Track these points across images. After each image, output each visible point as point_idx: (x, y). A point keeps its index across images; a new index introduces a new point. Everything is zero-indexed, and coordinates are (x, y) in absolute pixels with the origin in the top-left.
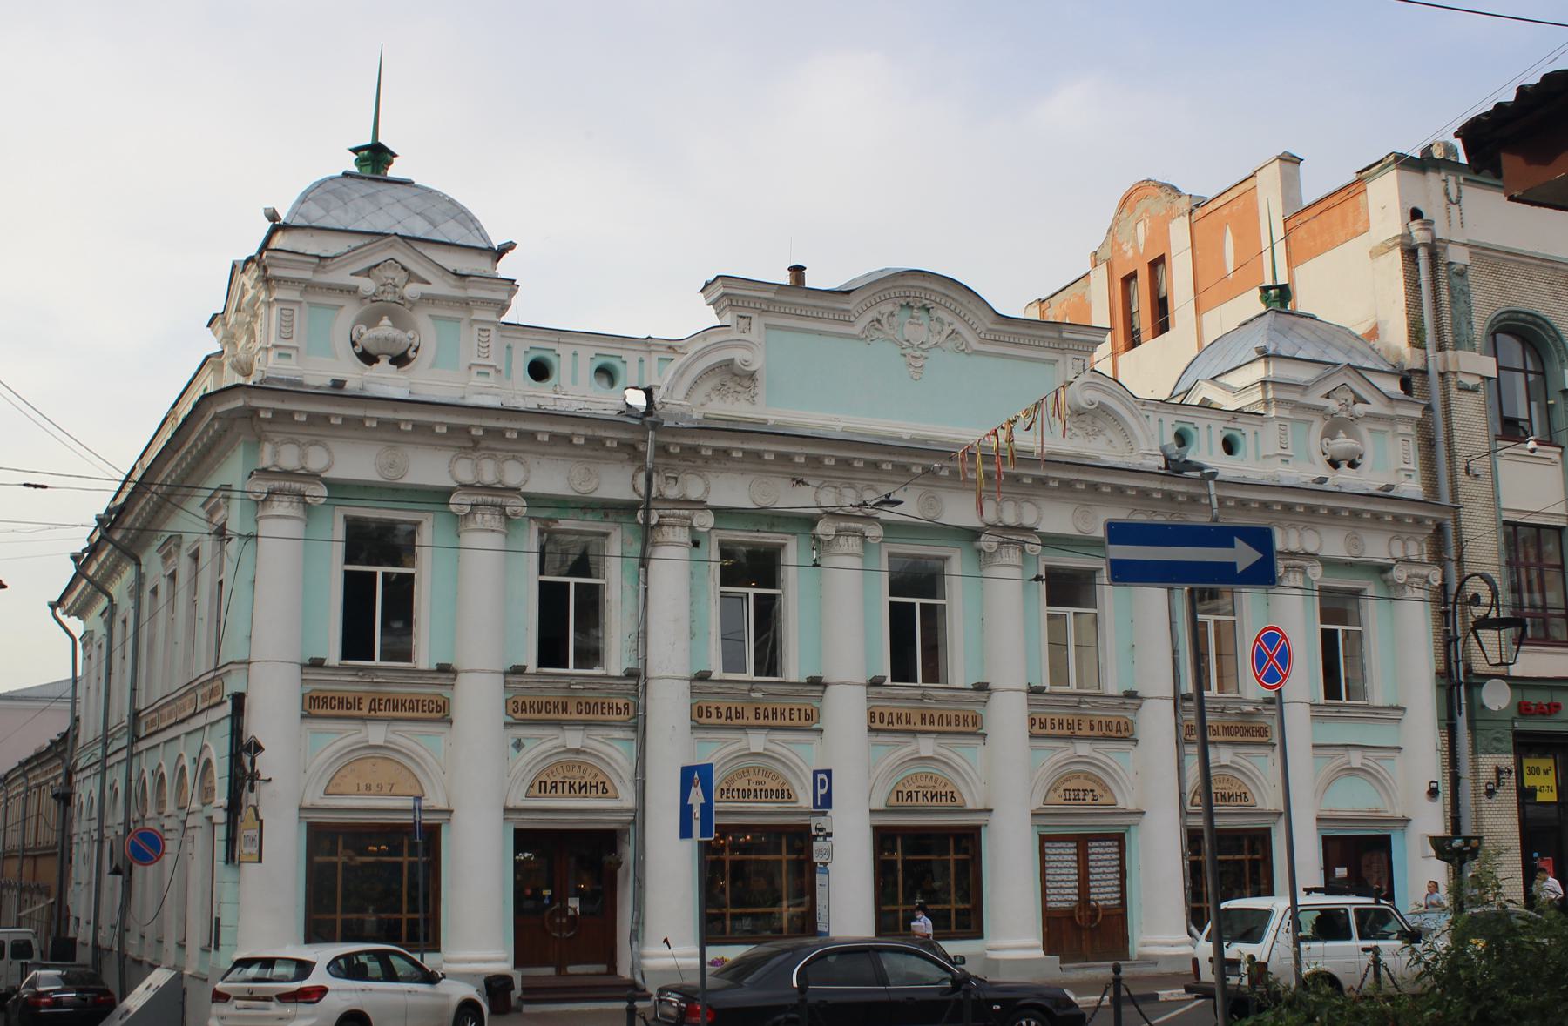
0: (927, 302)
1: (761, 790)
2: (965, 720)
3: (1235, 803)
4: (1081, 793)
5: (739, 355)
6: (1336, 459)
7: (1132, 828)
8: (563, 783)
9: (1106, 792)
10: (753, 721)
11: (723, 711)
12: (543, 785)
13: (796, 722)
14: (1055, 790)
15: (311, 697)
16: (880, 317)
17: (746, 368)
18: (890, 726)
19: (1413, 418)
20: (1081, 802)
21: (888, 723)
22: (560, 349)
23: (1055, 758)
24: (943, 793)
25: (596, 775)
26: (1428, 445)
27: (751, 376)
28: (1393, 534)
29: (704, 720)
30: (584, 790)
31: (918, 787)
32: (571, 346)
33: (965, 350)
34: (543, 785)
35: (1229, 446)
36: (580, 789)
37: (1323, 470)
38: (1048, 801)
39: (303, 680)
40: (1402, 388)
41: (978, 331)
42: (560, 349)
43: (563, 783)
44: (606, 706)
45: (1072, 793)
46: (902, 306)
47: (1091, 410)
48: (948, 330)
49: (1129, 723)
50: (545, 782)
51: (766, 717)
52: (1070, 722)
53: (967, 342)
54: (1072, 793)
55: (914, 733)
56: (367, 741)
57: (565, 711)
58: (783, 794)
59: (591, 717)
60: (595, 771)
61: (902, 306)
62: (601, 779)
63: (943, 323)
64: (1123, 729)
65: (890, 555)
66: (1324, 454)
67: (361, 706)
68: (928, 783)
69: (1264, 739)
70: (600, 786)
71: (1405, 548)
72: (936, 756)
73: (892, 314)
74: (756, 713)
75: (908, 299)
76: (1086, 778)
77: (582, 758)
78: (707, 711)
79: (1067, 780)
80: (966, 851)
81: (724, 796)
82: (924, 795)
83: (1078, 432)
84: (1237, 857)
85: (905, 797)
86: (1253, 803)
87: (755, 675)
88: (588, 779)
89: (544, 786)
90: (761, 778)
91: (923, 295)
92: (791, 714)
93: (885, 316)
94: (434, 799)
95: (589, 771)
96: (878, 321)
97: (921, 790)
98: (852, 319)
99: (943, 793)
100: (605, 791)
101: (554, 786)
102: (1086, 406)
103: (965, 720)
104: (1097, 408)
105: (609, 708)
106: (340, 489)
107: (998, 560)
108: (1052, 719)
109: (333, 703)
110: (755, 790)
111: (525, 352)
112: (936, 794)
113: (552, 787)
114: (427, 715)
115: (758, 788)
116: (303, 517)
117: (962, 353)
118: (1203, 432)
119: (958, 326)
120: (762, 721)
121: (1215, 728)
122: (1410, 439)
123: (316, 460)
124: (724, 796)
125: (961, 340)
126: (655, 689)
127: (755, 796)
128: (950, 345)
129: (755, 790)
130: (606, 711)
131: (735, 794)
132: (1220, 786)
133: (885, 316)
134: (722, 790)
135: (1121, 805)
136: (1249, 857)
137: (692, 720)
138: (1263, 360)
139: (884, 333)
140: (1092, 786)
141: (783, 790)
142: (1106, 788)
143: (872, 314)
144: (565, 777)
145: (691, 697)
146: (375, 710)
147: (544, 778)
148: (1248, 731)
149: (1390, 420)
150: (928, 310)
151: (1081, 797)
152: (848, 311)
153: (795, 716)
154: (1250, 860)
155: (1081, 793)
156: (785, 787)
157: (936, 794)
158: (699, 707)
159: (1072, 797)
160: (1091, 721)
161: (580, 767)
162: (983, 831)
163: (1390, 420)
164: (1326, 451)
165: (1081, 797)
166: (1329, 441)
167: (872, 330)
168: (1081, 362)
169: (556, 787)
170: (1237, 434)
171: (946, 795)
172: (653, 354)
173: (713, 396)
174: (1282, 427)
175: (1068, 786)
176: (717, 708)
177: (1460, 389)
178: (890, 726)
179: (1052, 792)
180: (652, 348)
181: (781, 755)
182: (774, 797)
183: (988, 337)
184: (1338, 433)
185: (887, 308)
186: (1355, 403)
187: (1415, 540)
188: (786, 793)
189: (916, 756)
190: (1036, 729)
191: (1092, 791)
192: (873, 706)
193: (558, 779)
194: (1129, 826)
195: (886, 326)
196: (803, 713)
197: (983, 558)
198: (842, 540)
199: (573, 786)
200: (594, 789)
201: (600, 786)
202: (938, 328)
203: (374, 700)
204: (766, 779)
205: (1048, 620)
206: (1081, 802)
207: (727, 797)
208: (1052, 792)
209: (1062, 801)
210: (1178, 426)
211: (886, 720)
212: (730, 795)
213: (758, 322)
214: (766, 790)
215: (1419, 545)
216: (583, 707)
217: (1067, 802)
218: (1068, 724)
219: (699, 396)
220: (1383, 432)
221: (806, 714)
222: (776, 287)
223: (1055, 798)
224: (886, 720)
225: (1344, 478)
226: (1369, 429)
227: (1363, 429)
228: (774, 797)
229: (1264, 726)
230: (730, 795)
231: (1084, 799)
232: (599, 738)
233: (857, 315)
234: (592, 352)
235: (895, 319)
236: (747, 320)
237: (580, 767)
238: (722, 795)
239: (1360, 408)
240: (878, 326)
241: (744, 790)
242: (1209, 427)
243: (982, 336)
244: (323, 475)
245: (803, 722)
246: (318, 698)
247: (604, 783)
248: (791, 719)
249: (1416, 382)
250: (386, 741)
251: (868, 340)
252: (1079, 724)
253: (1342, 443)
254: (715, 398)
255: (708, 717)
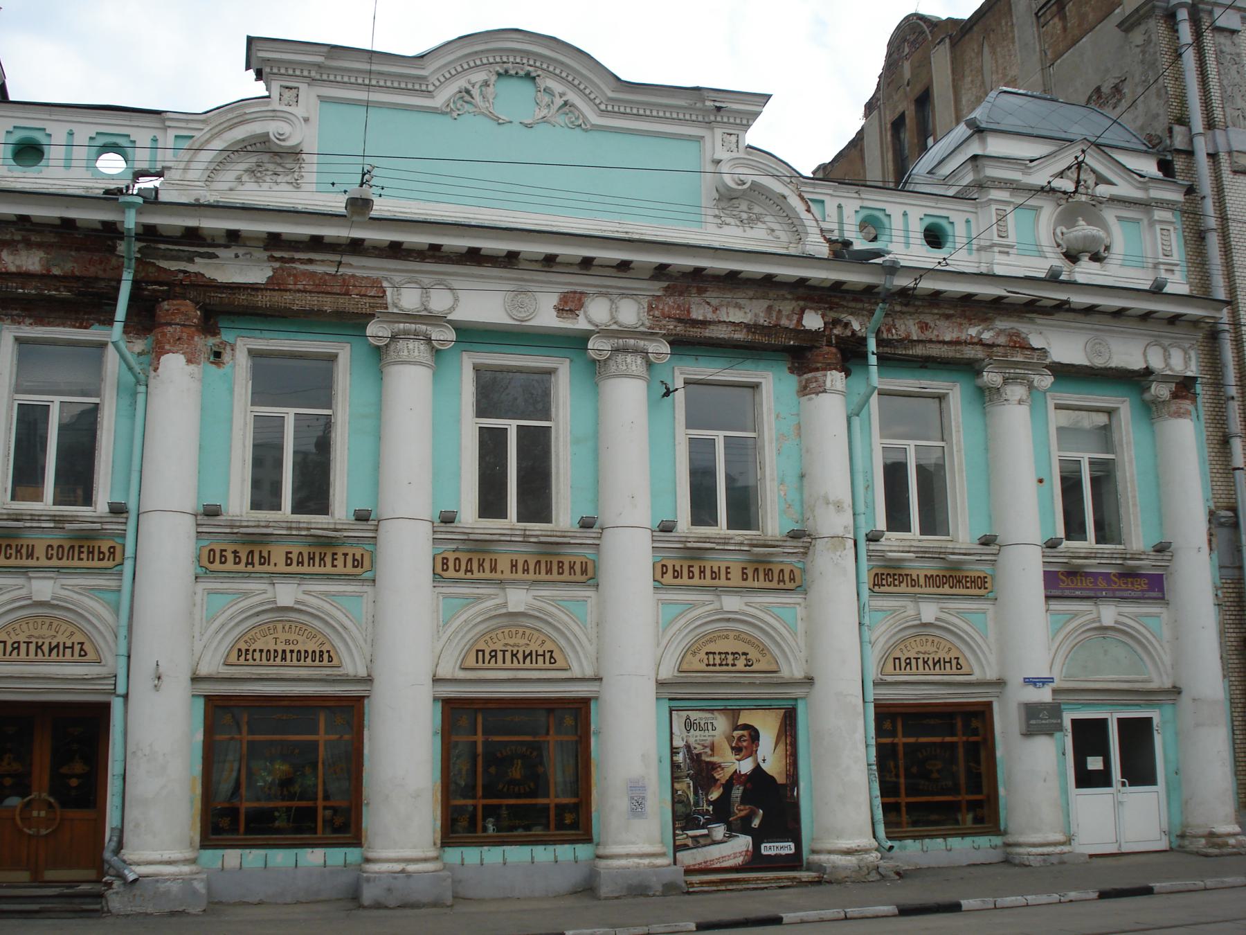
0: (531, 69)
1: (292, 651)
2: (572, 568)
3: (943, 671)
4: (730, 657)
5: (272, 128)
6: (1073, 253)
7: (799, 701)
8: (504, 652)
9: (764, 655)
10: (282, 568)
11: (294, 556)
12: (897, 661)
13: (340, 569)
14: (694, 654)
15: (926, 576)
16: (470, 87)
17: (283, 144)
18: (782, 585)
19: (1174, 203)
20: (730, 668)
21: (466, 571)
22: (51, 127)
23: (242, 605)
24: (540, 652)
25: (950, 650)
26: (1197, 238)
27: (295, 153)
28: (1152, 339)
29: (217, 566)
30: (55, 651)
31: (918, 653)
32: (92, 126)
33: (582, 126)
34: (897, 661)
35: (934, 237)
36: (525, 658)
37: (1055, 260)
38: (685, 667)
39: (198, 532)
40: (1159, 170)
41: (597, 101)
42: (51, 127)
43: (504, 652)
44: (85, 550)
45: (717, 657)
46: (499, 75)
47: (744, 190)
48: (559, 102)
49: (797, 573)
50: (899, 659)
51: (300, 563)
52: (677, 568)
53: (584, 116)
54: (717, 657)
55: (501, 583)
56: (275, 602)
57: (30, 555)
58: (321, 656)
59: (64, 562)
60: (71, 629)
61: (499, 75)
62: (549, 646)
63: (553, 95)
64: (787, 578)
65: (477, 369)
66: (1059, 245)
67: (729, 576)
68: (44, 631)
69: (982, 592)
70: (954, 662)
71: (1167, 357)
72: (531, 612)
73: (486, 84)
74: (287, 558)
75: (505, 65)
76: (737, 638)
77: (56, 613)
78: (221, 556)
79: (711, 641)
80: (975, 732)
81: (242, 658)
82: (925, 662)
83: (728, 220)
84: (948, 739)
85: (903, 665)
86: (564, 665)
87: (1097, 543)
88: (61, 639)
89: (484, 656)
90: (292, 637)
91: (525, 61)
92: (334, 559)
93: (477, 86)
94: (353, 665)
95: (63, 629)
96: (468, 92)
97: (921, 656)
98: (431, 88)
99: (540, 652)
100: (83, 653)
101: (16, 647)
102: (734, 186)
103: (572, 568)
104: (750, 188)
105: (89, 552)
106: (470, 334)
107: (613, 368)
108: (222, 551)
109: (9, 551)
110: (284, 651)
111: (921, 219)
112: (530, 654)
113: (907, 664)
114: (96, 563)
115: (288, 648)
116: (645, 374)
117: (578, 130)
118: (897, 222)
119: (572, 97)
120: (294, 568)
121: (915, 577)
122: (1171, 228)
123: (439, 302)
124: (242, 658)
125: (577, 113)
126: (151, 525)
127: (284, 659)
128: (562, 119)
129: (284, 651)
130: (84, 556)
131: (257, 655)
132: (511, 642)
133: (477, 86)
134: (240, 650)
135: (785, 673)
136: (964, 739)
137: (654, 581)
138: (976, 136)
139: (475, 106)
140: (740, 647)
141: (321, 651)
142: (763, 650)
143: (461, 83)
144: (506, 645)
145: (198, 538)
146: (878, 585)
147: (481, 646)
148: (959, 582)
149: (1146, 205)
150: (534, 78)
151: (730, 662)
152: (424, 78)
153: (340, 562)
154: (967, 743)
155: (730, 657)
156: (324, 649)
157: (530, 654)
158: (663, 566)
159: (718, 661)
160: (288, 553)
161: (51, 624)
162: (593, 705)
163: (1146, 205)
164: (1061, 242)
165: (730, 662)
166: (1065, 230)
167: (461, 102)
168: (733, 139)
169: (18, 648)
170: (944, 223)
171: (544, 655)
172: (169, 131)
173: (245, 178)
174: (1165, 232)
175: (711, 647)
176: (235, 552)
177: (1235, 172)
178: (782, 585)
179: (689, 656)
180: (168, 123)
181: (318, 609)
182: (309, 659)
183: (610, 108)
184: (1077, 221)
185: (479, 77)
186: (1097, 184)
187: (1179, 347)
188: (326, 656)
189: (504, 611)
190: (668, 578)
191: (744, 654)
192: (664, 558)
193: (22, 638)
194: (796, 699)
195: (478, 99)
196: (350, 559)
197: (596, 369)
198: (401, 344)
199: (515, 655)
200: (68, 651)
201: (77, 648)
202: (547, 99)
203: (877, 574)
204: (298, 638)
205: (883, 451)
206: (730, 668)
207: (246, 660)
208: (689, 656)
209: (703, 667)
210: (928, 221)
211: (463, 567)
212: (249, 657)
213: (308, 95)
214: (299, 651)
215: (1185, 352)
216: (54, 552)
217: (711, 668)
218: (712, 572)
219: (227, 177)
220: (1137, 221)
221: (354, 560)
222: (325, 49)
223: (696, 663)
224: (463, 567)
225: (1086, 271)
226: (1119, 218)
227: (1110, 215)
228: (309, 659)
229: (982, 575)
230: (249, 657)
231: (734, 665)
232: (76, 589)
233: (437, 83)
234: (921, 212)
235: (491, 89)
236: (294, 91)
237: (51, 624)
238: (239, 656)
239: (1103, 190)
240: (467, 98)
241: (268, 651)
242: (905, 214)
243: (603, 107)
244: (449, 317)
245: (350, 569)
246: (932, 576)
247: (82, 644)
248: (728, 579)
249: (1179, 164)
250: (937, 619)
251: (455, 115)
252: (727, 573)
253: (1083, 229)
254: (251, 186)
255: (221, 563)
